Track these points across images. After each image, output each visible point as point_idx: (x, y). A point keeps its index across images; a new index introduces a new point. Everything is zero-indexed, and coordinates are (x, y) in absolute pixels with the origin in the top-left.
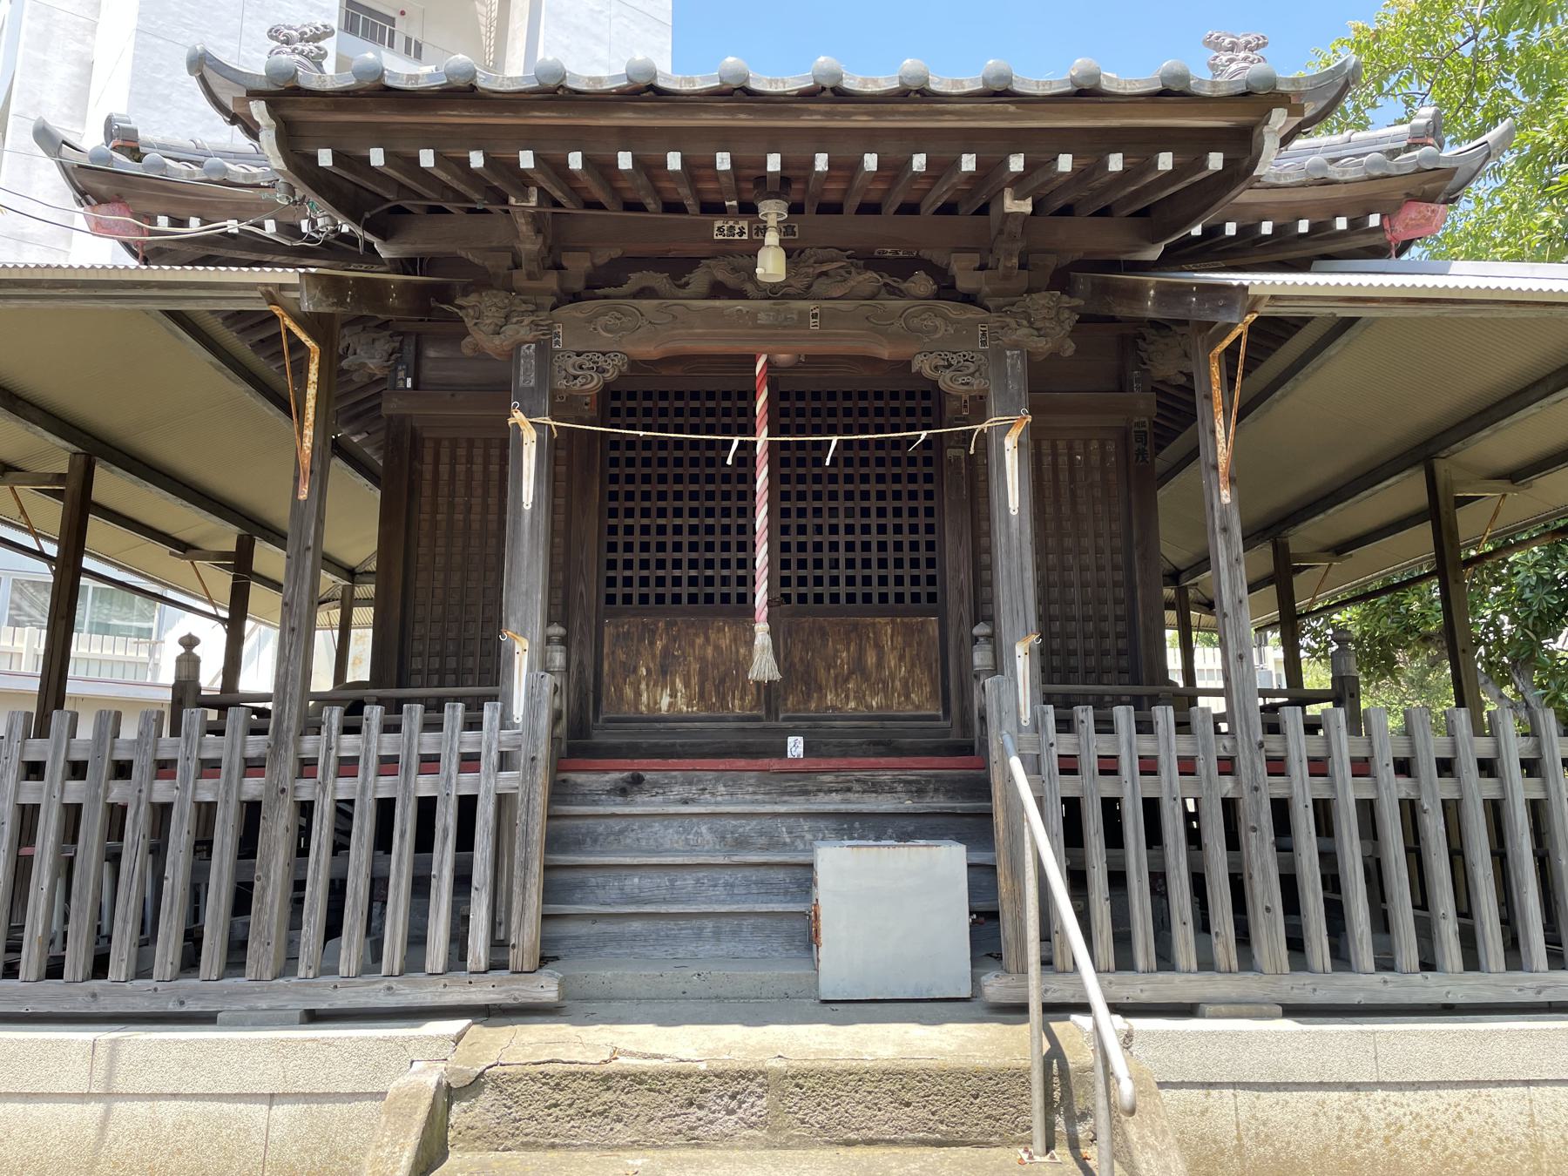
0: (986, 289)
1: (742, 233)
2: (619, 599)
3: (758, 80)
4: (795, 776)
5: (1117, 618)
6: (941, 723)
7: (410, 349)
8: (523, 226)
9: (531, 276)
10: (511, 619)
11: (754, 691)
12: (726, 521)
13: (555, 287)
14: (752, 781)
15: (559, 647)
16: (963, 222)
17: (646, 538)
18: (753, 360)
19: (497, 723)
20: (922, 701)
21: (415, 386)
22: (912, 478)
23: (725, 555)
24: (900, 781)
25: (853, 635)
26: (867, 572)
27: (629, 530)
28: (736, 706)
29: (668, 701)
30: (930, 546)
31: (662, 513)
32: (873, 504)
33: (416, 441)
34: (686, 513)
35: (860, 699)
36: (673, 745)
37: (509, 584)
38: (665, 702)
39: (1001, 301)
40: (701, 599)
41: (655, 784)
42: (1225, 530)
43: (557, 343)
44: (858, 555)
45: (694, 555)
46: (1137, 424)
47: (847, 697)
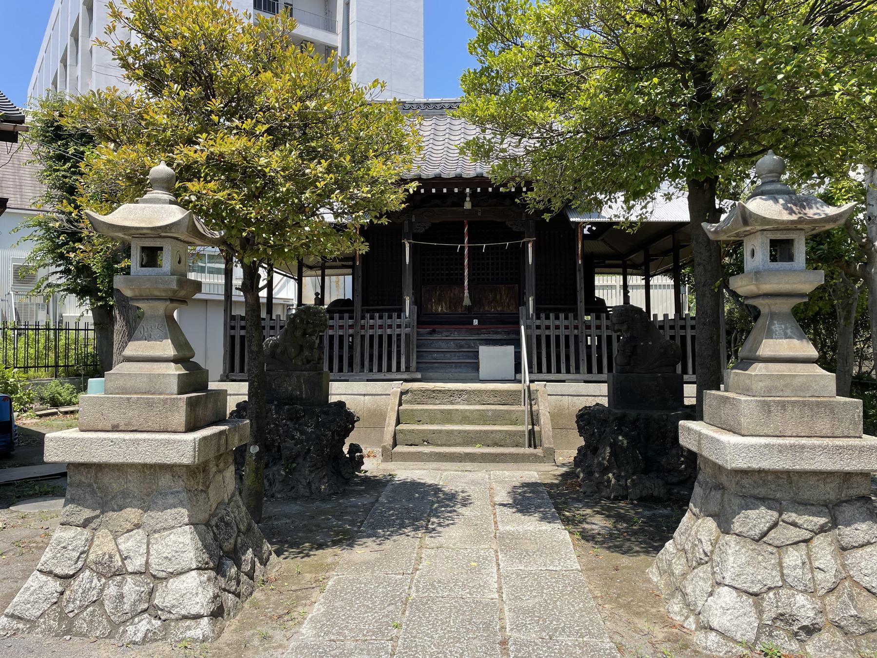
28: (460, 310)
38: (440, 309)
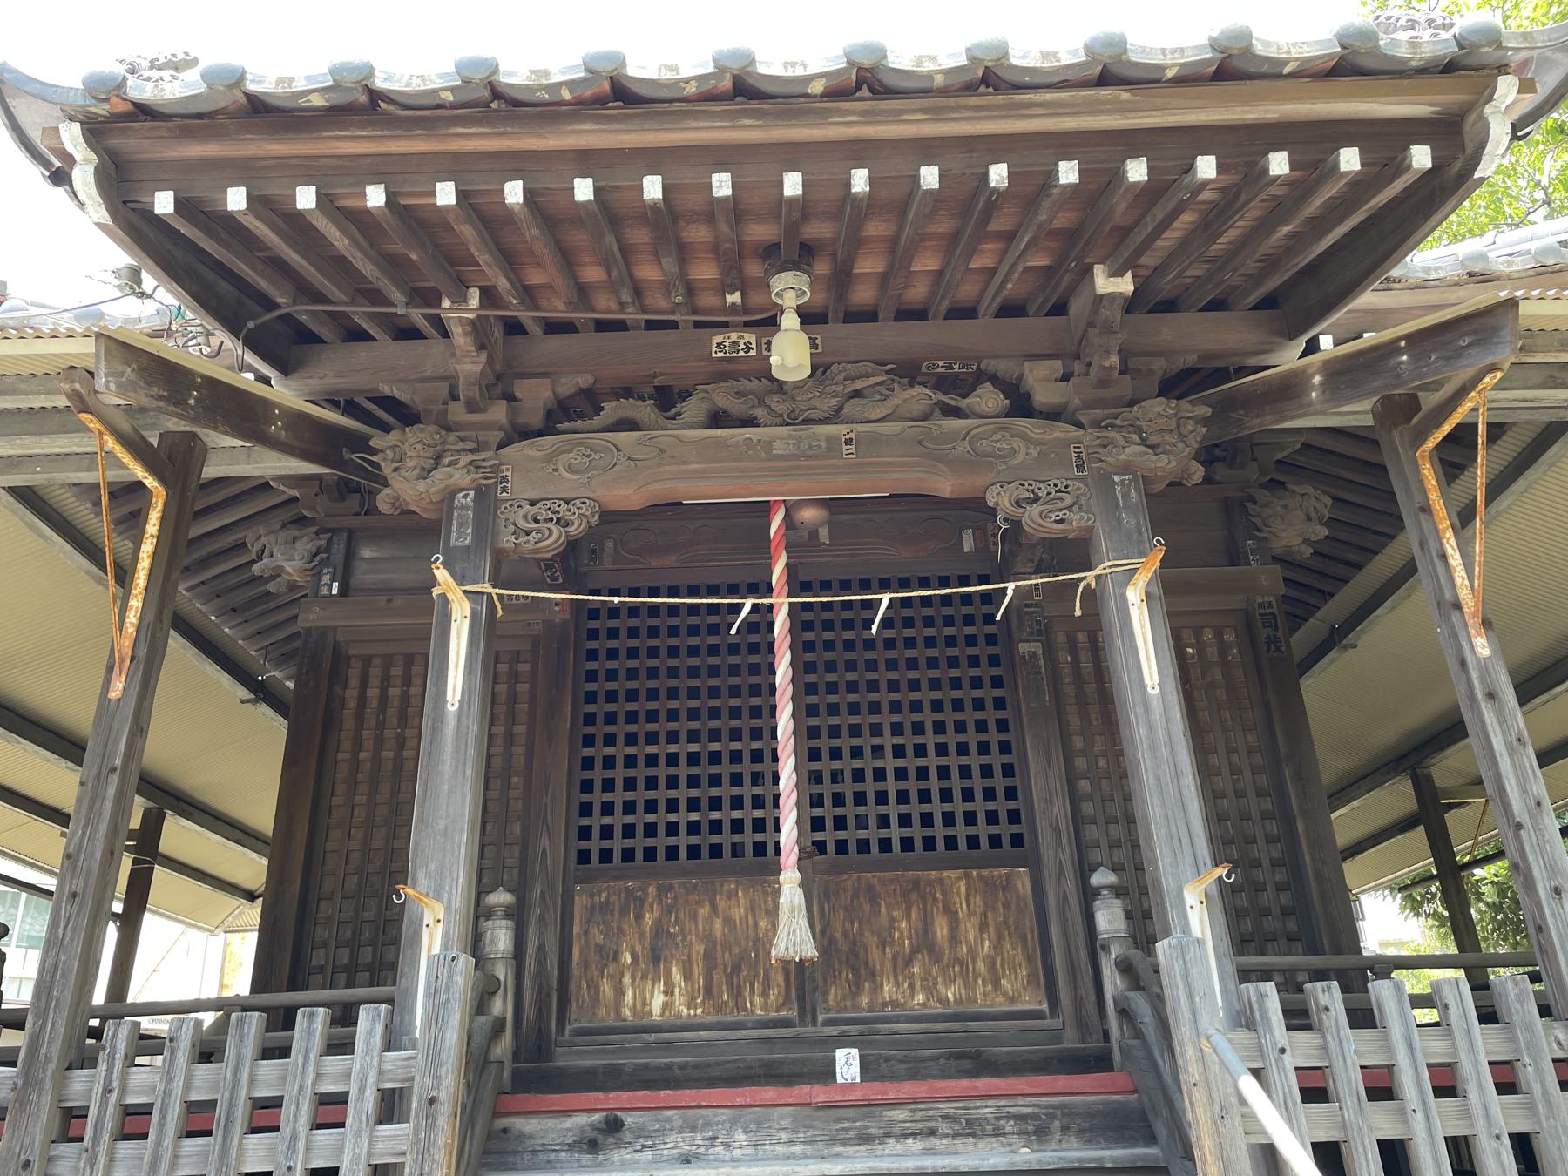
0: (1077, 401)
1: (748, 349)
2: (595, 857)
3: (768, 64)
4: (850, 1112)
5: (1274, 863)
6: (1047, 1022)
7: (339, 549)
8: (460, 338)
9: (472, 407)
10: (421, 874)
11: (780, 979)
12: (736, 746)
13: (504, 420)
14: (786, 1122)
15: (504, 922)
16: (1036, 327)
17: (631, 773)
18: (765, 509)
19: (378, 1040)
20: (1017, 991)
21: (344, 591)
22: (976, 683)
23: (736, 791)
24: (1009, 1116)
25: (914, 897)
26: (926, 808)
27: (609, 762)
28: (757, 1005)
29: (660, 1000)
30: (1008, 770)
31: (652, 738)
32: (928, 717)
33: (339, 659)
34: (684, 737)
35: (930, 989)
36: (669, 1067)
37: (421, 820)
38: (657, 1001)
39: (1097, 413)
40: (705, 852)
41: (640, 1132)
42: (1491, 695)
43: (504, 489)
44: (913, 785)
45: (694, 793)
46: (1261, 605)
47: (912, 987)
